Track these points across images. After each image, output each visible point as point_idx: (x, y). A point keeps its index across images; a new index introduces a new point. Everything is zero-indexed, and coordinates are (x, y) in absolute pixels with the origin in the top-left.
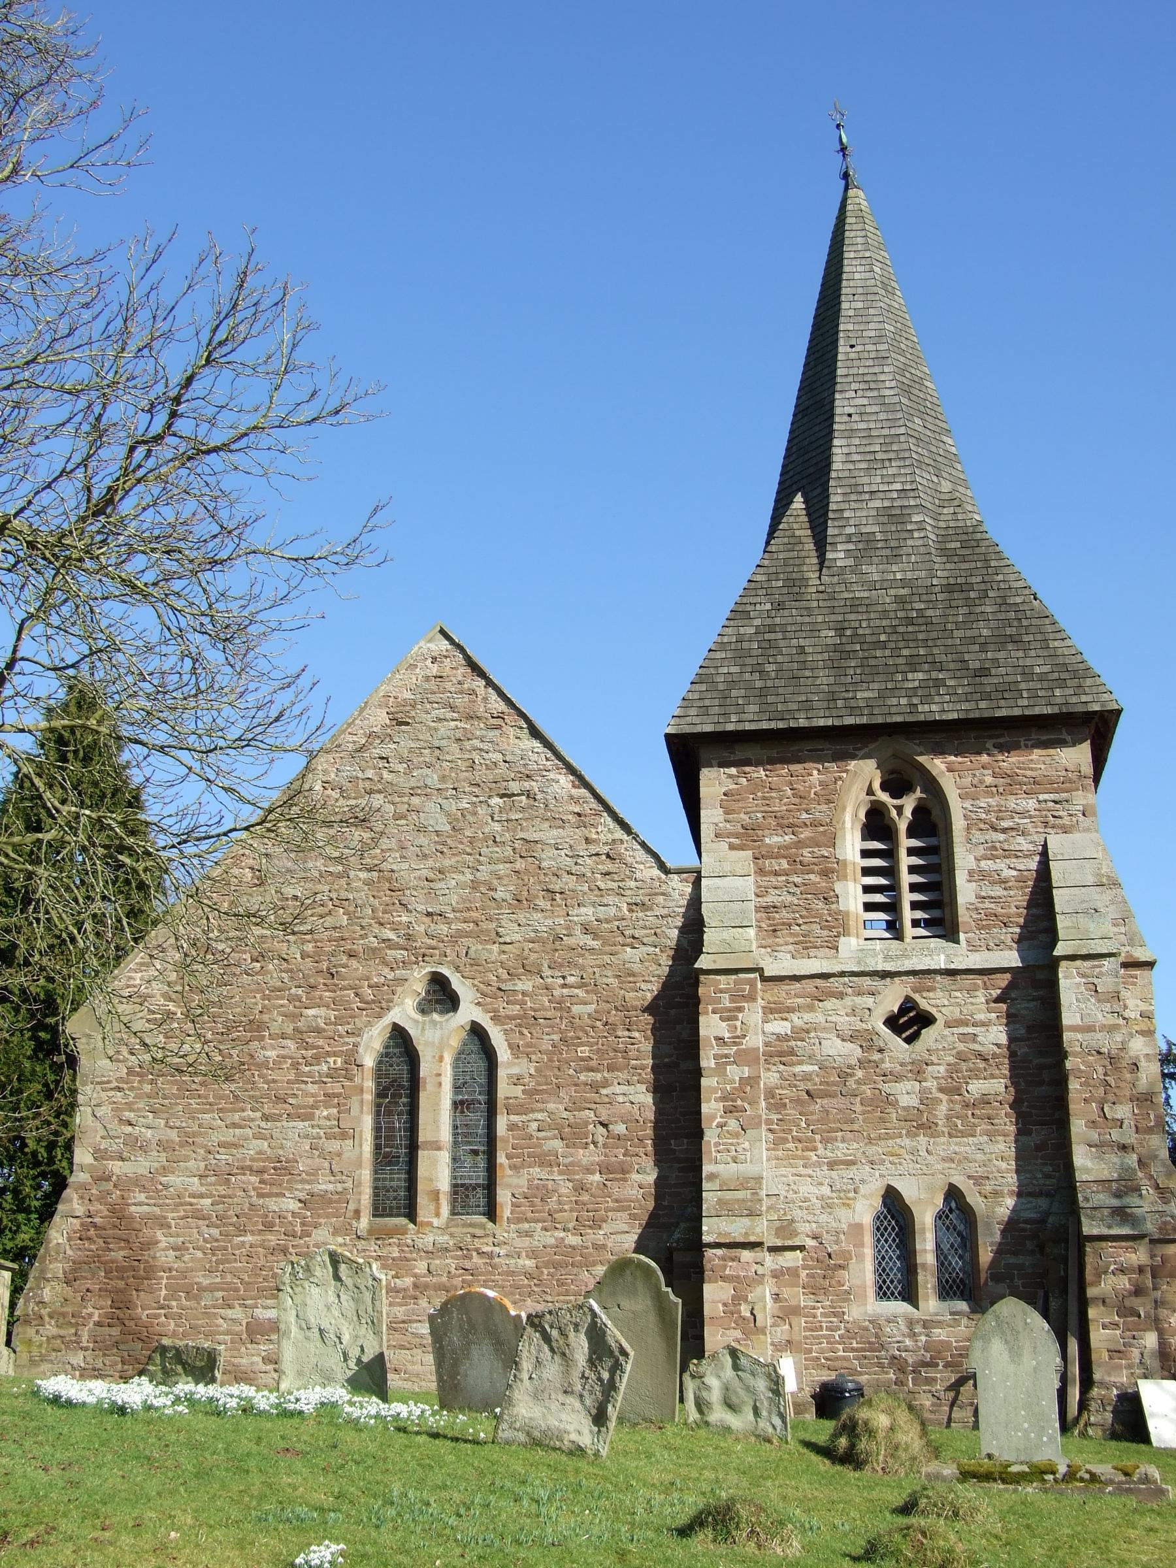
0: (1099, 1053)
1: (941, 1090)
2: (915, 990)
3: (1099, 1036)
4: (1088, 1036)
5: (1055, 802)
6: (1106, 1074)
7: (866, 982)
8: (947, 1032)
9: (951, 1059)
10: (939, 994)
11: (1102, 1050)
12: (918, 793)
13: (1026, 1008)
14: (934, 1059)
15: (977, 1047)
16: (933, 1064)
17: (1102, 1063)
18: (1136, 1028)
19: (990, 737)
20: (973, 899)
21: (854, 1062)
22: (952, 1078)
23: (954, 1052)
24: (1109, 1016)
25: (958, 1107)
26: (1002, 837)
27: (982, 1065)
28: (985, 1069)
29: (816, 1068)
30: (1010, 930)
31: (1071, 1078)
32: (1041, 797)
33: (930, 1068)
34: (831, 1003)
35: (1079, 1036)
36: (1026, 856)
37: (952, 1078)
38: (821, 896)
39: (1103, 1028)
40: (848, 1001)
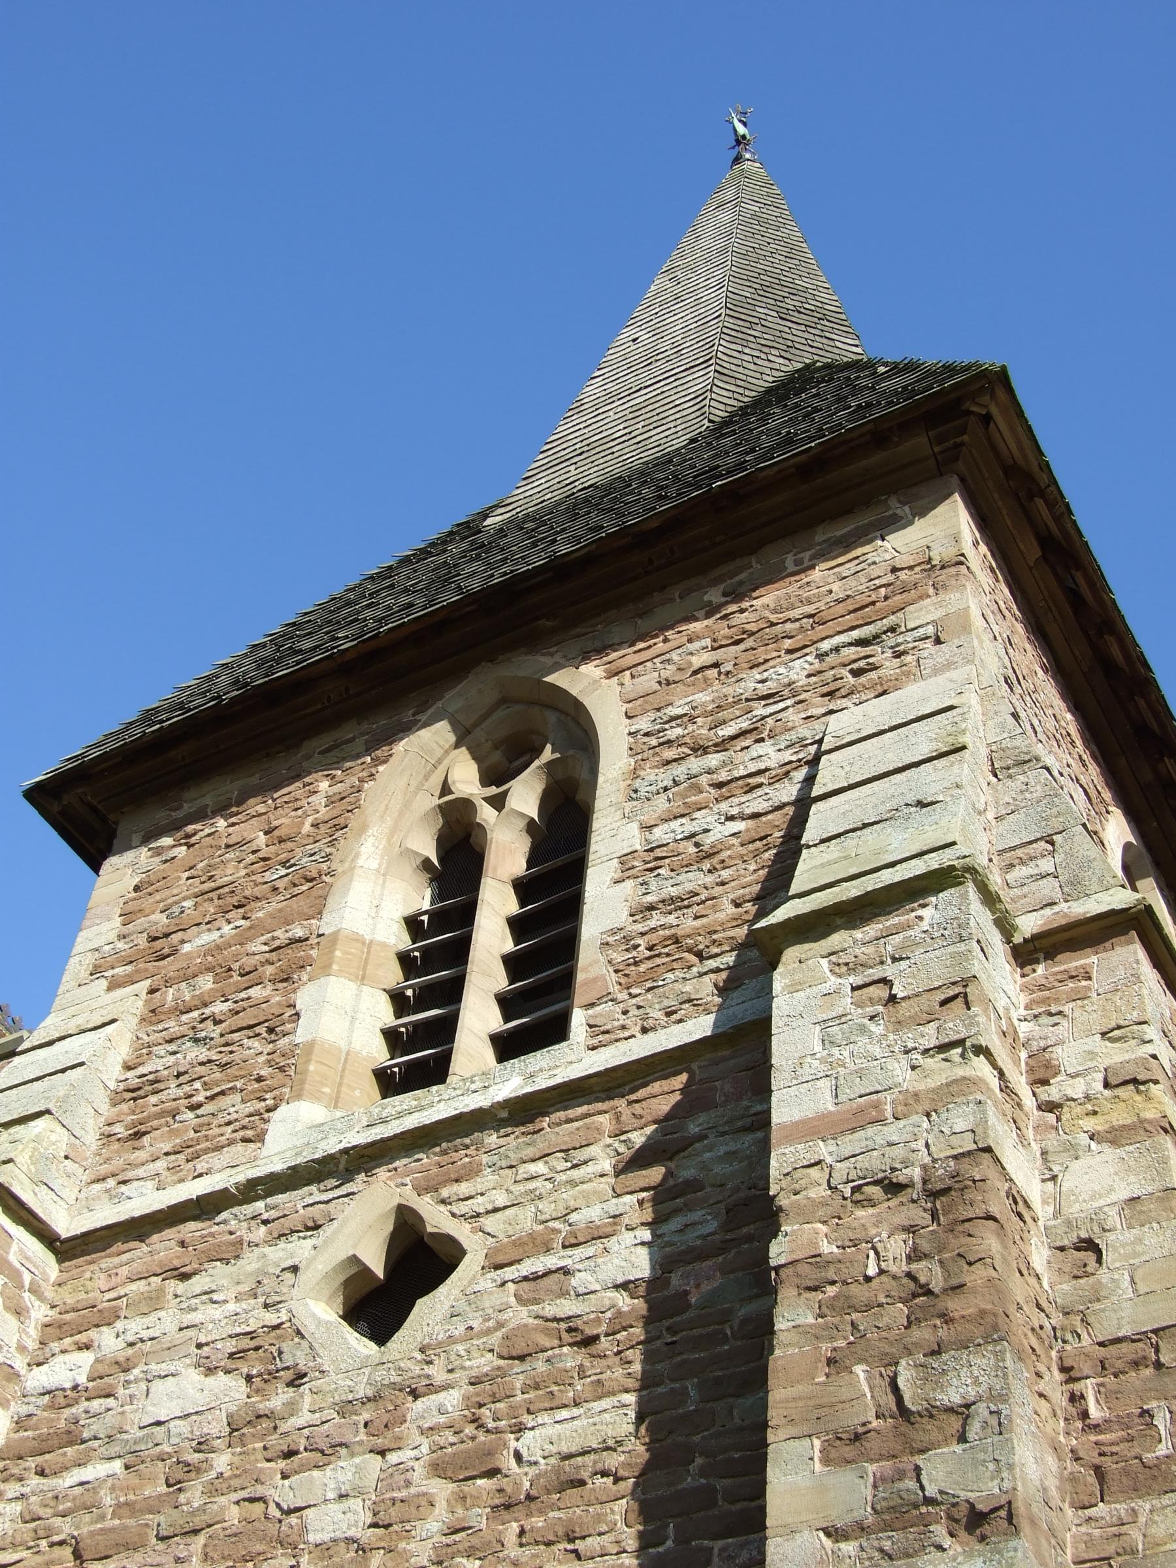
0: (893, 1188)
1: (438, 1469)
2: (421, 1190)
3: (893, 1131)
4: (851, 1143)
5: (862, 642)
6: (915, 1255)
7: (294, 1201)
8: (486, 1282)
9: (484, 1363)
10: (487, 1179)
11: (900, 1177)
12: (548, 754)
13: (732, 1155)
14: (438, 1373)
15: (567, 1307)
16: (432, 1389)
17: (900, 1219)
18: (1090, 1124)
19: (715, 583)
20: (621, 917)
21: (216, 1426)
22: (475, 1420)
23: (495, 1339)
24: (933, 1063)
25: (479, 1517)
26: (713, 760)
27: (571, 1358)
28: (582, 1373)
29: (117, 1466)
30: (712, 964)
31: (787, 1295)
32: (825, 646)
33: (420, 1404)
34: (216, 1275)
35: (824, 1150)
36: (778, 779)
37: (475, 1420)
38: (261, 1029)
39: (909, 1102)
40: (250, 1263)
